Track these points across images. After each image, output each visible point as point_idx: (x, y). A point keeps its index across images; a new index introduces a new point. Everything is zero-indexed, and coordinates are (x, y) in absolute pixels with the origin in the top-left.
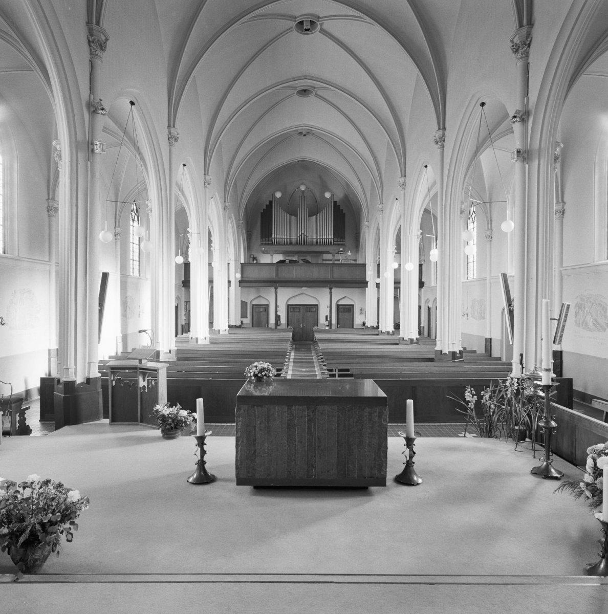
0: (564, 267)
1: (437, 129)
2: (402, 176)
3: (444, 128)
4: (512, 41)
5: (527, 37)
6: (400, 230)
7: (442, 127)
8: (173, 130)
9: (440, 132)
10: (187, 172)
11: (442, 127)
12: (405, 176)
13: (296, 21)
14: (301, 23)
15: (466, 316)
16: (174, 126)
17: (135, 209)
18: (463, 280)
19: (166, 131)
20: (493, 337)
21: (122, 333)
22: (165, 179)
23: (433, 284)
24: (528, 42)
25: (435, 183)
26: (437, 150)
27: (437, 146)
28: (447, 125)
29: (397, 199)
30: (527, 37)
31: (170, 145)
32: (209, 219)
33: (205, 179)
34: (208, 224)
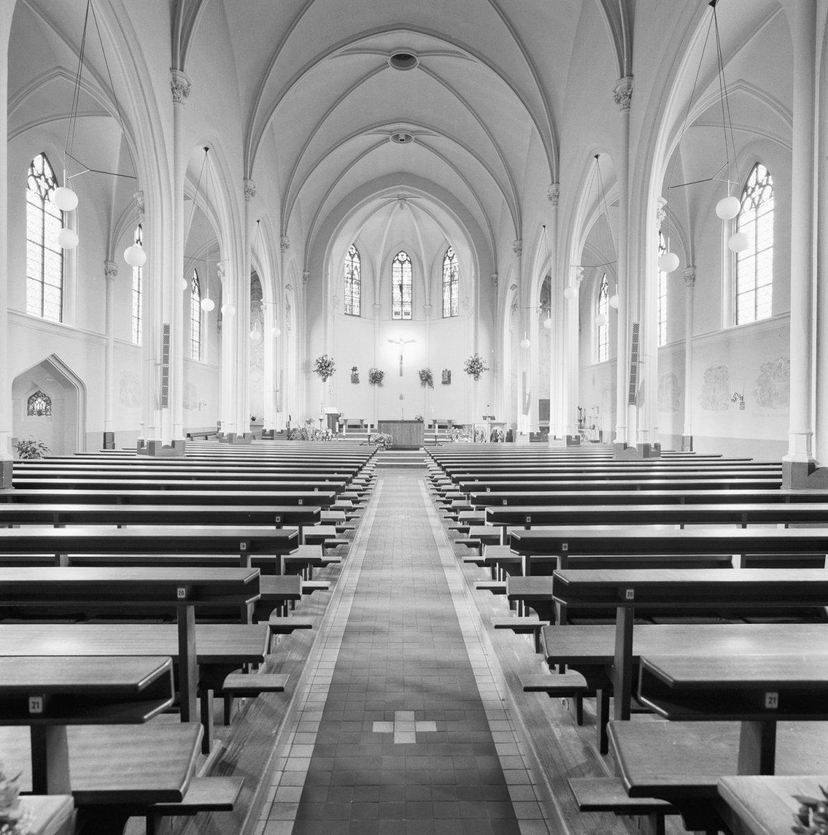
0: (782, 315)
1: (550, 182)
2: (553, 183)
3: (631, 75)
4: (615, 91)
5: (628, 89)
6: (548, 278)
7: (627, 72)
8: (284, 239)
9: (554, 187)
10: (212, 163)
11: (627, 72)
12: (558, 183)
13: (390, 56)
14: (397, 136)
15: (739, 401)
16: (182, 70)
17: (195, 278)
18: (725, 326)
19: (168, 76)
20: (693, 435)
21: (667, 341)
22: (167, 166)
23: (252, 442)
24: (629, 93)
25: (612, 181)
26: (617, 112)
27: (551, 203)
28: (634, 71)
29: (544, 227)
30: (628, 89)
31: (247, 200)
32: (253, 252)
33: (175, 80)
34: (251, 260)
